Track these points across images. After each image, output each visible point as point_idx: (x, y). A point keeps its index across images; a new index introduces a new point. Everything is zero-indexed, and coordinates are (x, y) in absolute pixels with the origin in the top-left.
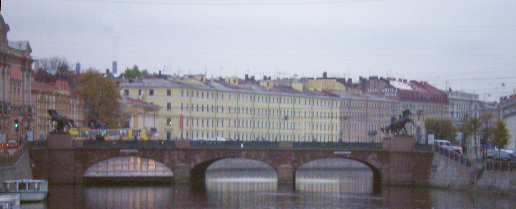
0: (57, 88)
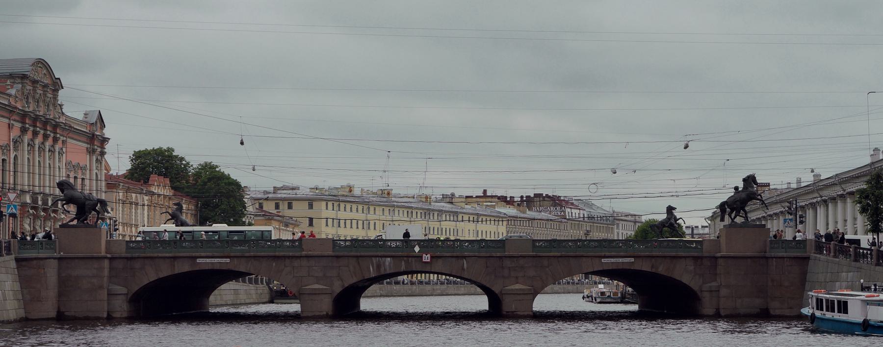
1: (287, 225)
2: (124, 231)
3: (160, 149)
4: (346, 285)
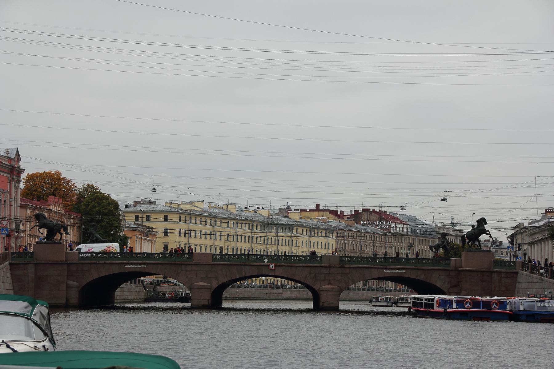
0: (50, 205)
1: (147, 235)
2: (30, 241)
3: (50, 172)
4: (220, 283)
